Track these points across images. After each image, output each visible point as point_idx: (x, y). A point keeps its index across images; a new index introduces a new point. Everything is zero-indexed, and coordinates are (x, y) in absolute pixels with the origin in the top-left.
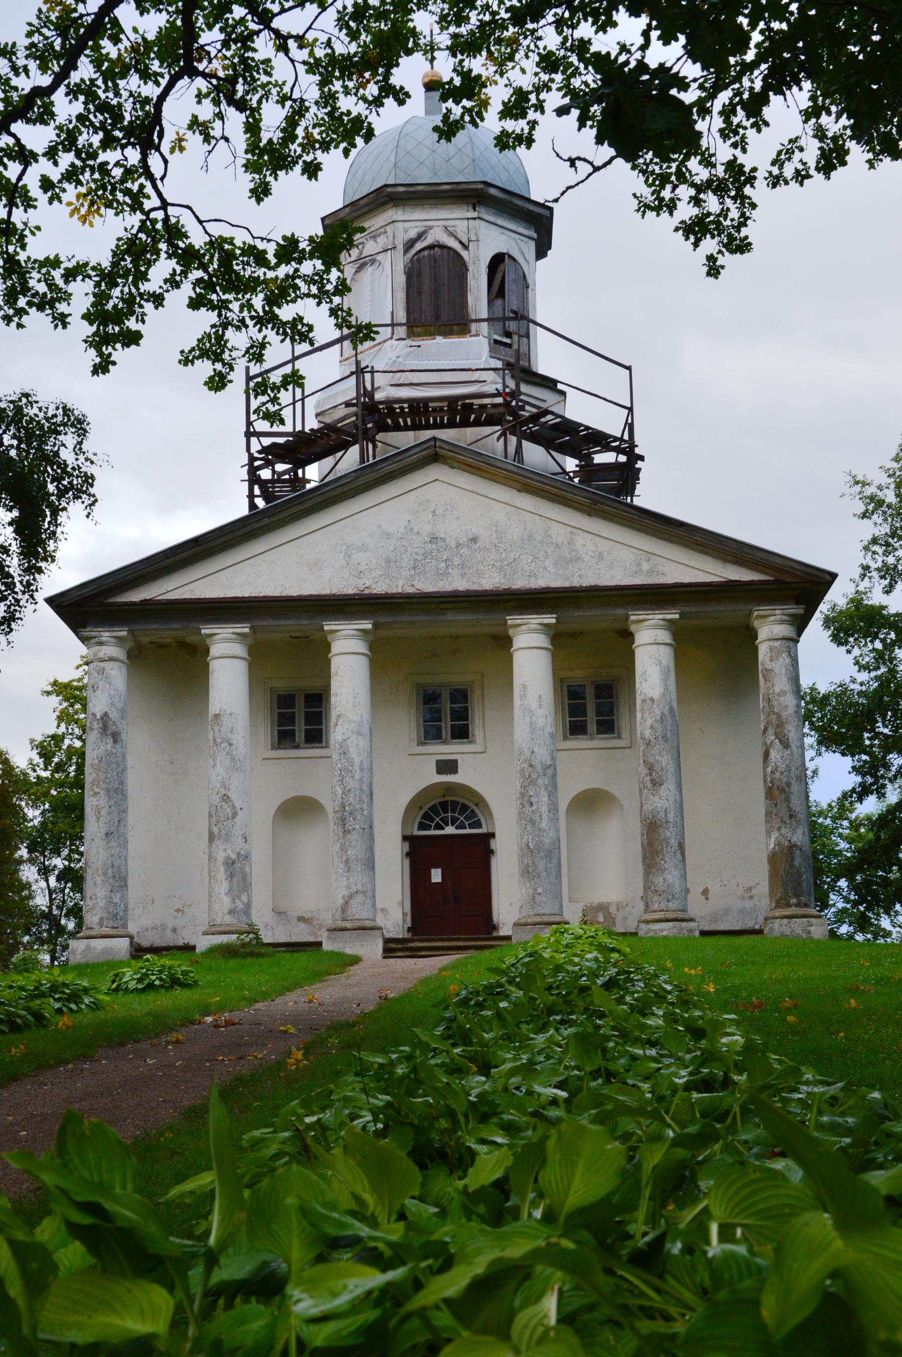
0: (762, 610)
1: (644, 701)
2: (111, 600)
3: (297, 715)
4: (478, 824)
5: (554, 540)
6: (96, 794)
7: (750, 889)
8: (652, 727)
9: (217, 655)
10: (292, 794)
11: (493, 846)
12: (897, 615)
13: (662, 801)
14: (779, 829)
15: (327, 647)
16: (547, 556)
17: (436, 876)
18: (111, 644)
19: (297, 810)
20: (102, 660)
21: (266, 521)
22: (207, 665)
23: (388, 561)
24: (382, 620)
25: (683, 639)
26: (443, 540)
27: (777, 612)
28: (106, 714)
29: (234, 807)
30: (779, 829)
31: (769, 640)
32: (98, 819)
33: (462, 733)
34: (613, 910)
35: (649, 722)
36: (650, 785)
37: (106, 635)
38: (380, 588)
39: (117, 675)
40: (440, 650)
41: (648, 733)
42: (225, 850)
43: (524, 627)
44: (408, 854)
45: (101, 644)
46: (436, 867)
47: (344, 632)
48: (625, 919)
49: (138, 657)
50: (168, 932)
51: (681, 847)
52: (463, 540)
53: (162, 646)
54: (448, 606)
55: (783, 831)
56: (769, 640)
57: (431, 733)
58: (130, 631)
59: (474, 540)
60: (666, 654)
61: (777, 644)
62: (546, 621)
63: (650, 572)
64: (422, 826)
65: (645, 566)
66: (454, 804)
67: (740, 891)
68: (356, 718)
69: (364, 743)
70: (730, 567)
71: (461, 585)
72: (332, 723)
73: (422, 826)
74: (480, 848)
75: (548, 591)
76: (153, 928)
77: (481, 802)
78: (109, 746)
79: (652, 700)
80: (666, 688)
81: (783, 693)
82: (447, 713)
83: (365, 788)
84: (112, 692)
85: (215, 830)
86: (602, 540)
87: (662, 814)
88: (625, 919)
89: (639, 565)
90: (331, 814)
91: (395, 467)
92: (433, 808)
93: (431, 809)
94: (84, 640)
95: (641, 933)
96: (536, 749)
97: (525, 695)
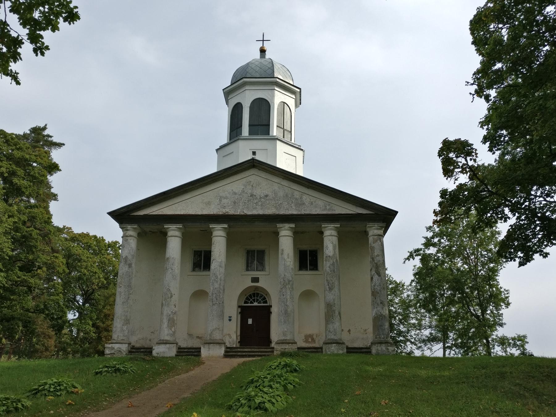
0: (370, 224)
1: (326, 257)
4: (266, 302)
5: (295, 197)
6: (121, 287)
7: (366, 330)
8: (329, 267)
13: (330, 297)
16: (292, 203)
17: (250, 321)
19: (200, 295)
20: (127, 236)
21: (191, 187)
22: (166, 239)
23: (235, 203)
25: (343, 240)
26: (255, 196)
28: (127, 256)
29: (171, 294)
33: (261, 266)
34: (314, 337)
35: (328, 265)
36: (328, 289)
37: (129, 227)
38: (232, 212)
39: (133, 243)
40: (252, 235)
44: (240, 313)
45: (127, 230)
46: (250, 318)
49: (141, 235)
50: (148, 341)
51: (340, 314)
52: (262, 195)
53: (153, 233)
55: (378, 309)
57: (248, 267)
58: (183, 226)
59: (267, 196)
60: (335, 240)
61: (376, 237)
63: (329, 210)
64: (245, 302)
65: (328, 207)
66: (258, 294)
68: (220, 260)
69: (222, 270)
71: (261, 212)
73: (245, 302)
74: (267, 311)
75: (292, 215)
77: (267, 293)
79: (329, 256)
80: (335, 252)
82: (256, 258)
83: (221, 287)
85: (164, 302)
88: (319, 341)
89: (326, 207)
92: (250, 296)
95: (154, 353)
96: (286, 274)
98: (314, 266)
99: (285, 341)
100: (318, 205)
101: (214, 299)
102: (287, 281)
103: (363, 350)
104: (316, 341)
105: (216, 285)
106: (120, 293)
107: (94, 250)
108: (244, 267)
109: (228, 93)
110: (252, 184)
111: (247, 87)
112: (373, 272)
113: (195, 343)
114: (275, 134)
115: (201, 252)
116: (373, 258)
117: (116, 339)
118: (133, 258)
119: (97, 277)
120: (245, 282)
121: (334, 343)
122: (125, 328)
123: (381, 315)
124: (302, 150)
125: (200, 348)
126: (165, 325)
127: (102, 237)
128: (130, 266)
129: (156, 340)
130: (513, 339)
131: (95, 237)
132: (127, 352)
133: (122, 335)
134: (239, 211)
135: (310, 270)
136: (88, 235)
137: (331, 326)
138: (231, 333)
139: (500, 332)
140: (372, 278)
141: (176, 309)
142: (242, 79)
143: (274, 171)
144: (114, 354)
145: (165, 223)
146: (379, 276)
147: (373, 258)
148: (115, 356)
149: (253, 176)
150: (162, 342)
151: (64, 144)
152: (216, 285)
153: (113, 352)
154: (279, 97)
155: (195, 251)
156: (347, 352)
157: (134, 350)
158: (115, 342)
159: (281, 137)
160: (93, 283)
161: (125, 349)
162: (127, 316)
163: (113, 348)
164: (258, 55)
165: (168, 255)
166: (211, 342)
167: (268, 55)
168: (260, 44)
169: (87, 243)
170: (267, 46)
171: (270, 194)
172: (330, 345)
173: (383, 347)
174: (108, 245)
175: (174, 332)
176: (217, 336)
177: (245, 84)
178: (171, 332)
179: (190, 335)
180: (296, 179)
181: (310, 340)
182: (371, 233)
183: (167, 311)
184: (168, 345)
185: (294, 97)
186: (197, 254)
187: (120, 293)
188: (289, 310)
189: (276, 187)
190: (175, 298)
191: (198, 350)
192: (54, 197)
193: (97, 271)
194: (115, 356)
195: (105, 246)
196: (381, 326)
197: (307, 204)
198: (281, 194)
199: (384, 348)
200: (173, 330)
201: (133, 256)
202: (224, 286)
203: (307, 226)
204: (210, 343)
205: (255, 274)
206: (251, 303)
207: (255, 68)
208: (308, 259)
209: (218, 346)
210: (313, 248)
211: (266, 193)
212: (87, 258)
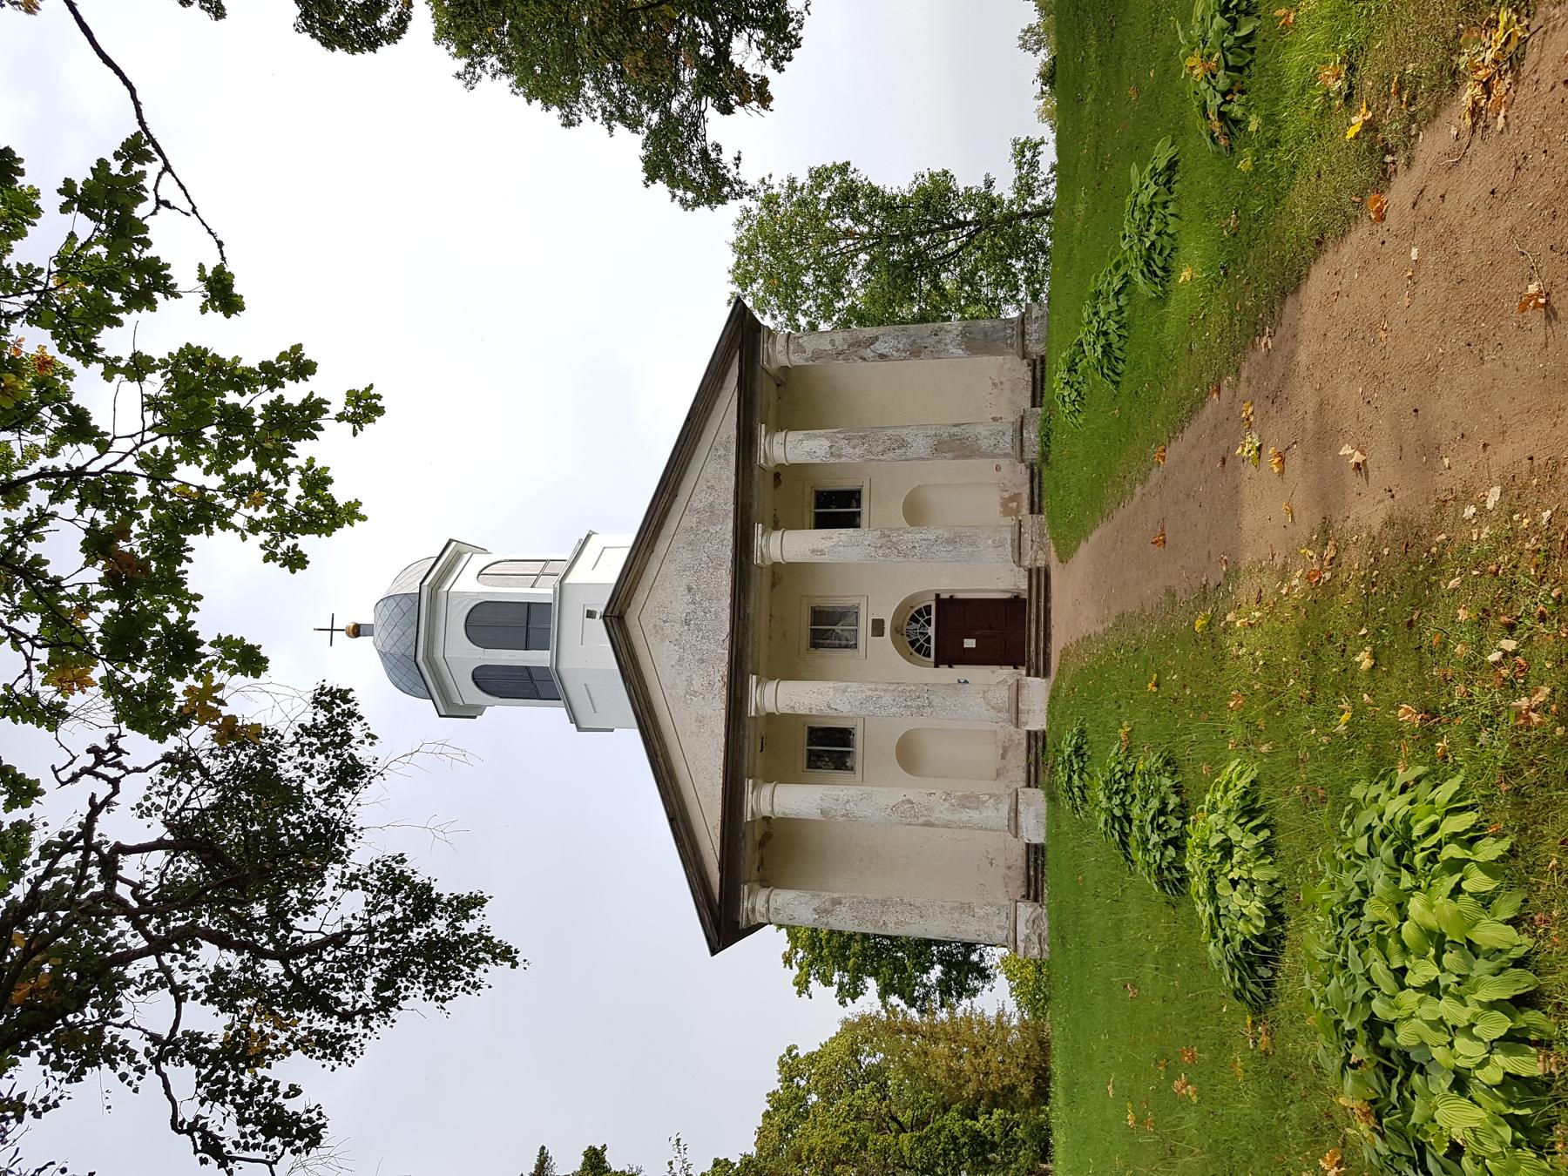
0: (763, 357)
2: (717, 891)
3: (830, 748)
12: (1043, 9)
13: (920, 445)
15: (770, 716)
17: (970, 643)
19: (908, 755)
20: (768, 910)
21: (660, 759)
23: (702, 661)
24: (750, 667)
25: (785, 423)
33: (845, 615)
34: (1006, 495)
37: (746, 905)
38: (723, 668)
40: (774, 623)
45: (753, 910)
50: (1010, 873)
52: (688, 598)
59: (690, 589)
60: (793, 436)
63: (727, 449)
65: (722, 452)
68: (831, 692)
69: (854, 686)
73: (922, 650)
82: (828, 629)
85: (922, 820)
91: (624, 651)
95: (1038, 838)
98: (853, 497)
100: (715, 474)
101: (919, 702)
102: (883, 540)
103: (1038, 374)
105: (888, 699)
108: (849, 652)
109: (451, 709)
111: (439, 654)
112: (868, 353)
114: (551, 591)
116: (839, 354)
123: (963, 334)
124: (588, 536)
125: (1029, 732)
126: (975, 816)
137: (985, 444)
139: (1005, 189)
140: (882, 357)
143: (634, 571)
147: (839, 354)
148: (1045, 934)
149: (643, 621)
152: (888, 699)
153: (1035, 939)
154: (467, 585)
159: (555, 580)
164: (365, 642)
165: (815, 814)
167: (367, 618)
168: (340, 637)
170: (343, 622)
171: (685, 581)
172: (1026, 444)
173: (1032, 328)
175: (991, 796)
176: (1002, 695)
179: (999, 774)
180: (652, 528)
181: (1014, 505)
182: (782, 360)
183: (942, 813)
184: (1021, 807)
185: (466, 557)
186: (815, 761)
188: (946, 535)
189: (670, 568)
190: (912, 794)
191: (1032, 736)
194: (1045, 934)
196: (986, 335)
198: (686, 556)
203: (760, 497)
204: (1015, 826)
205: (865, 627)
206: (928, 641)
208: (837, 508)
209: (1024, 691)
210: (810, 499)
211: (682, 590)
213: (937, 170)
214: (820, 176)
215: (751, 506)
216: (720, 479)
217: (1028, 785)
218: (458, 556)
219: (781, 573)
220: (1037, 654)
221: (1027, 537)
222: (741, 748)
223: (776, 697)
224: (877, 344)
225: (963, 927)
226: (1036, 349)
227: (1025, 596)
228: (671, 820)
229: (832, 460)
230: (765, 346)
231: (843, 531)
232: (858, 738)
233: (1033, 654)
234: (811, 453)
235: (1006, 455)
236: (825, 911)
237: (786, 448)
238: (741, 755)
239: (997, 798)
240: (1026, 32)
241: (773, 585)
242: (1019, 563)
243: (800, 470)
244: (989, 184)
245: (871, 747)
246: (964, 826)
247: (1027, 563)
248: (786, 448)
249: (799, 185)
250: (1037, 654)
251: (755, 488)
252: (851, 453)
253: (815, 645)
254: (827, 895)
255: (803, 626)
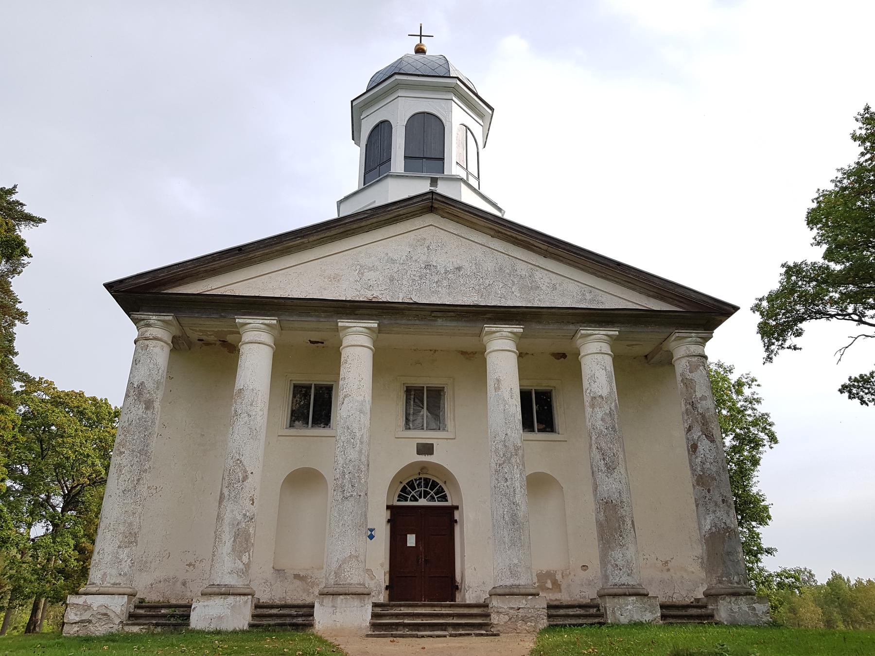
0: (683, 333)
2: (170, 291)
4: (444, 498)
5: (518, 272)
6: (122, 453)
7: (667, 562)
9: (247, 341)
10: (299, 466)
11: (457, 517)
13: (610, 486)
14: (714, 512)
17: (411, 540)
18: (160, 327)
19: (303, 480)
20: (147, 339)
23: (392, 279)
24: (386, 322)
26: (436, 267)
27: (693, 335)
28: (142, 383)
29: (246, 471)
30: (714, 512)
31: (688, 356)
32: (119, 476)
34: (558, 577)
35: (600, 415)
37: (153, 318)
40: (432, 354)
41: (599, 424)
42: (232, 511)
43: (497, 334)
45: (149, 325)
47: (354, 329)
48: (569, 586)
49: (179, 345)
50: (179, 584)
52: (450, 267)
53: (208, 344)
54: (439, 314)
55: (718, 514)
56: (688, 356)
58: (279, 321)
59: (459, 269)
61: (695, 359)
62: (515, 330)
63: (592, 301)
65: (588, 297)
67: (659, 564)
69: (366, 420)
70: (652, 300)
72: (340, 399)
73: (401, 498)
76: (165, 580)
77: (449, 477)
78: (140, 412)
79: (601, 397)
80: (611, 389)
81: (703, 398)
82: (424, 402)
83: (363, 459)
84: (151, 366)
85: (226, 492)
86: (554, 275)
87: (617, 495)
88: (569, 586)
90: (331, 484)
93: (425, 479)
94: (136, 321)
95: (197, 621)
96: (509, 432)
97: (499, 389)
99: (516, 591)
101: (348, 486)
104: (563, 587)
106: (120, 467)
107: (89, 419)
108: (402, 422)
110: (427, 243)
112: (697, 433)
113: (295, 595)
115: (309, 387)
117: (98, 582)
118: (158, 388)
119: (90, 462)
120: (399, 453)
121: (630, 595)
122: (123, 554)
125: (313, 607)
127: (106, 399)
128: (149, 405)
129: (203, 586)
130: (778, 575)
131: (94, 399)
132: (124, 618)
133: (114, 572)
134: (401, 296)
135: (539, 431)
136: (81, 394)
137: (617, 555)
138: (373, 565)
141: (254, 509)
142: (387, 83)
143: (475, 220)
144: (90, 622)
145: (236, 315)
146: (713, 441)
149: (429, 230)
150: (216, 590)
151: (44, 221)
152: (353, 454)
153: (86, 616)
154: (457, 117)
155: (295, 386)
156: (664, 617)
157: (142, 612)
158: (94, 589)
160: (82, 474)
161: (118, 611)
162: (131, 524)
163: (89, 607)
166: (341, 590)
169: (78, 407)
171: (466, 265)
172: (621, 600)
173: (743, 605)
174: (115, 413)
175: (247, 566)
176: (354, 577)
177: (398, 86)
178: (241, 566)
179: (279, 572)
180: (520, 237)
183: (232, 512)
184: (231, 599)
185: (481, 122)
186: (300, 391)
187: (120, 467)
188: (521, 514)
189: (478, 252)
192: (22, 316)
193: (91, 453)
194: (91, 628)
195: (109, 413)
196: (729, 553)
197: (544, 288)
198: (489, 265)
199: (745, 608)
200: (245, 559)
201: (158, 383)
202: (368, 456)
207: (414, 64)
208: (538, 411)
210: (543, 386)
211: (458, 262)
212: (76, 430)
213: (771, 512)
214: (762, 422)
215: (540, 322)
216: (563, 295)
217: (257, 607)
218: (481, 115)
219: (475, 359)
220: (397, 616)
221: (522, 602)
222: (308, 314)
223: (357, 345)
224: (706, 442)
225: (108, 535)
226: (723, 610)
227: (459, 600)
228: (240, 249)
229: (587, 399)
230: (694, 335)
231: (519, 409)
232: (320, 431)
233: (397, 611)
234: (593, 378)
235: (606, 577)
236: (140, 394)
237: (596, 355)
238: (300, 314)
239: (246, 571)
240: (810, 573)
241: (463, 353)
242: (494, 593)
243: (576, 373)
244: (769, 551)
245: (310, 446)
246: (217, 537)
247: (495, 602)
248: (596, 358)
249: (756, 406)
250: (397, 616)
251: (556, 326)
252: (596, 418)
253: (409, 390)
254: (158, 396)
255: (426, 380)
